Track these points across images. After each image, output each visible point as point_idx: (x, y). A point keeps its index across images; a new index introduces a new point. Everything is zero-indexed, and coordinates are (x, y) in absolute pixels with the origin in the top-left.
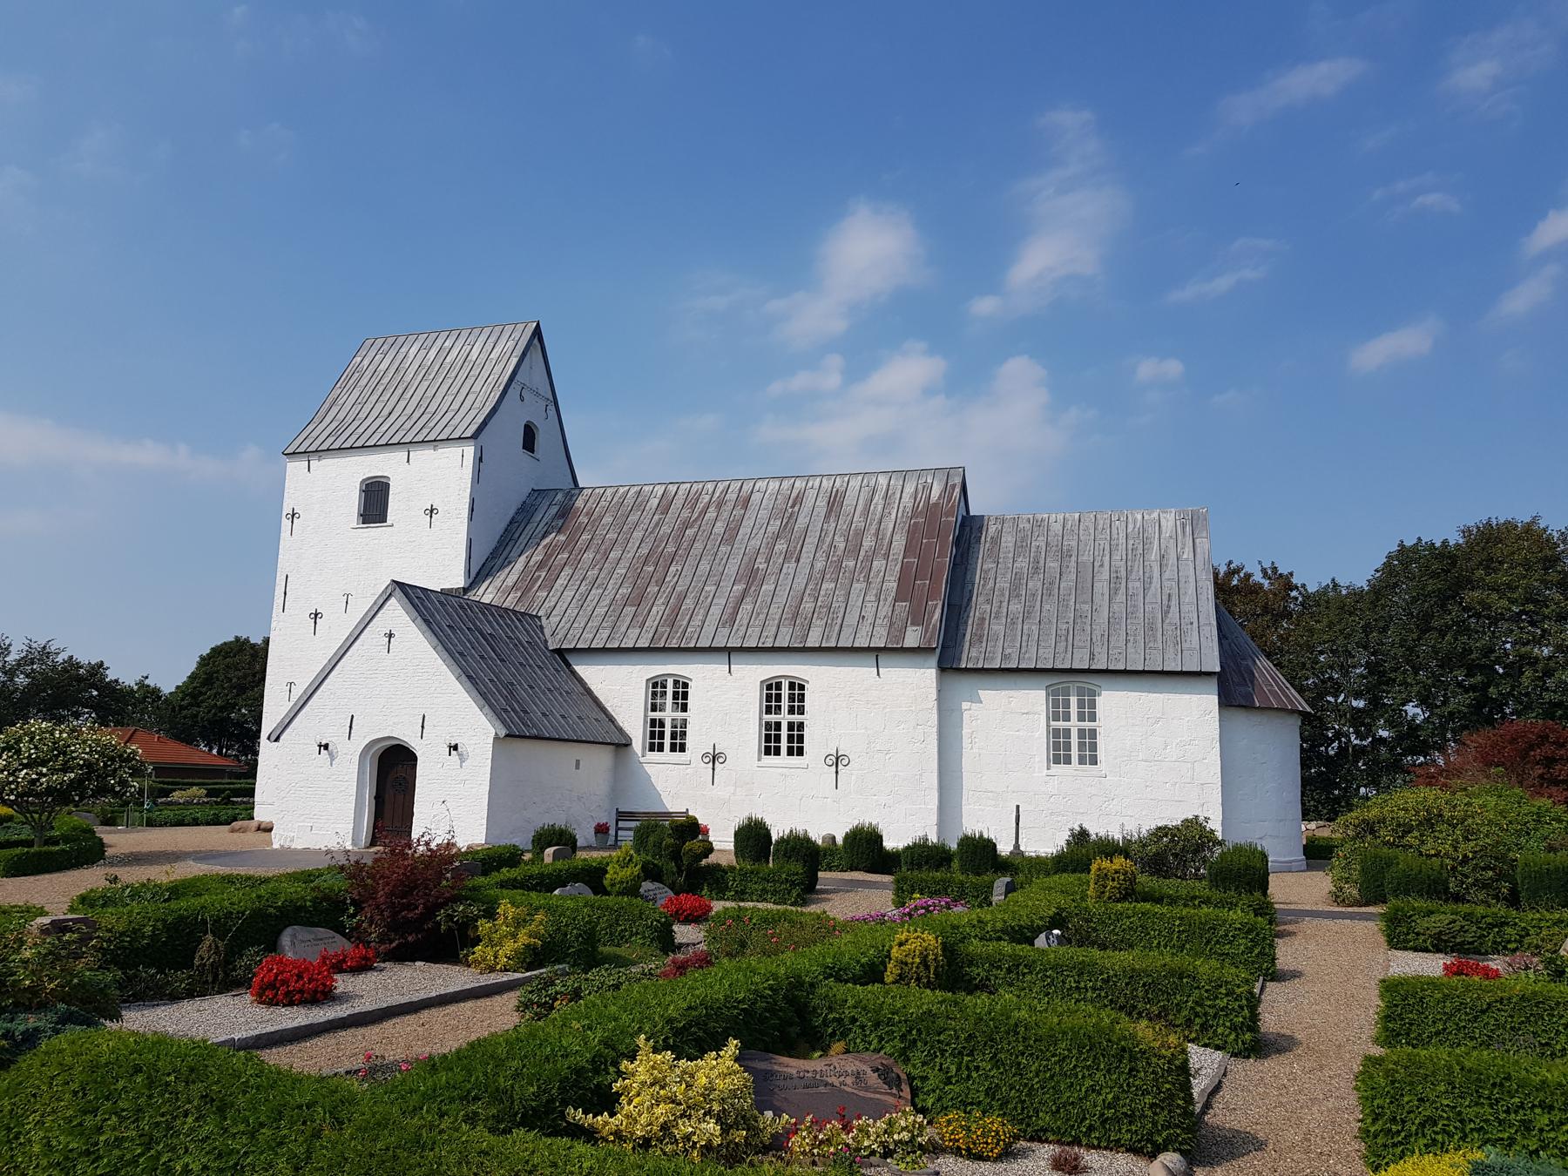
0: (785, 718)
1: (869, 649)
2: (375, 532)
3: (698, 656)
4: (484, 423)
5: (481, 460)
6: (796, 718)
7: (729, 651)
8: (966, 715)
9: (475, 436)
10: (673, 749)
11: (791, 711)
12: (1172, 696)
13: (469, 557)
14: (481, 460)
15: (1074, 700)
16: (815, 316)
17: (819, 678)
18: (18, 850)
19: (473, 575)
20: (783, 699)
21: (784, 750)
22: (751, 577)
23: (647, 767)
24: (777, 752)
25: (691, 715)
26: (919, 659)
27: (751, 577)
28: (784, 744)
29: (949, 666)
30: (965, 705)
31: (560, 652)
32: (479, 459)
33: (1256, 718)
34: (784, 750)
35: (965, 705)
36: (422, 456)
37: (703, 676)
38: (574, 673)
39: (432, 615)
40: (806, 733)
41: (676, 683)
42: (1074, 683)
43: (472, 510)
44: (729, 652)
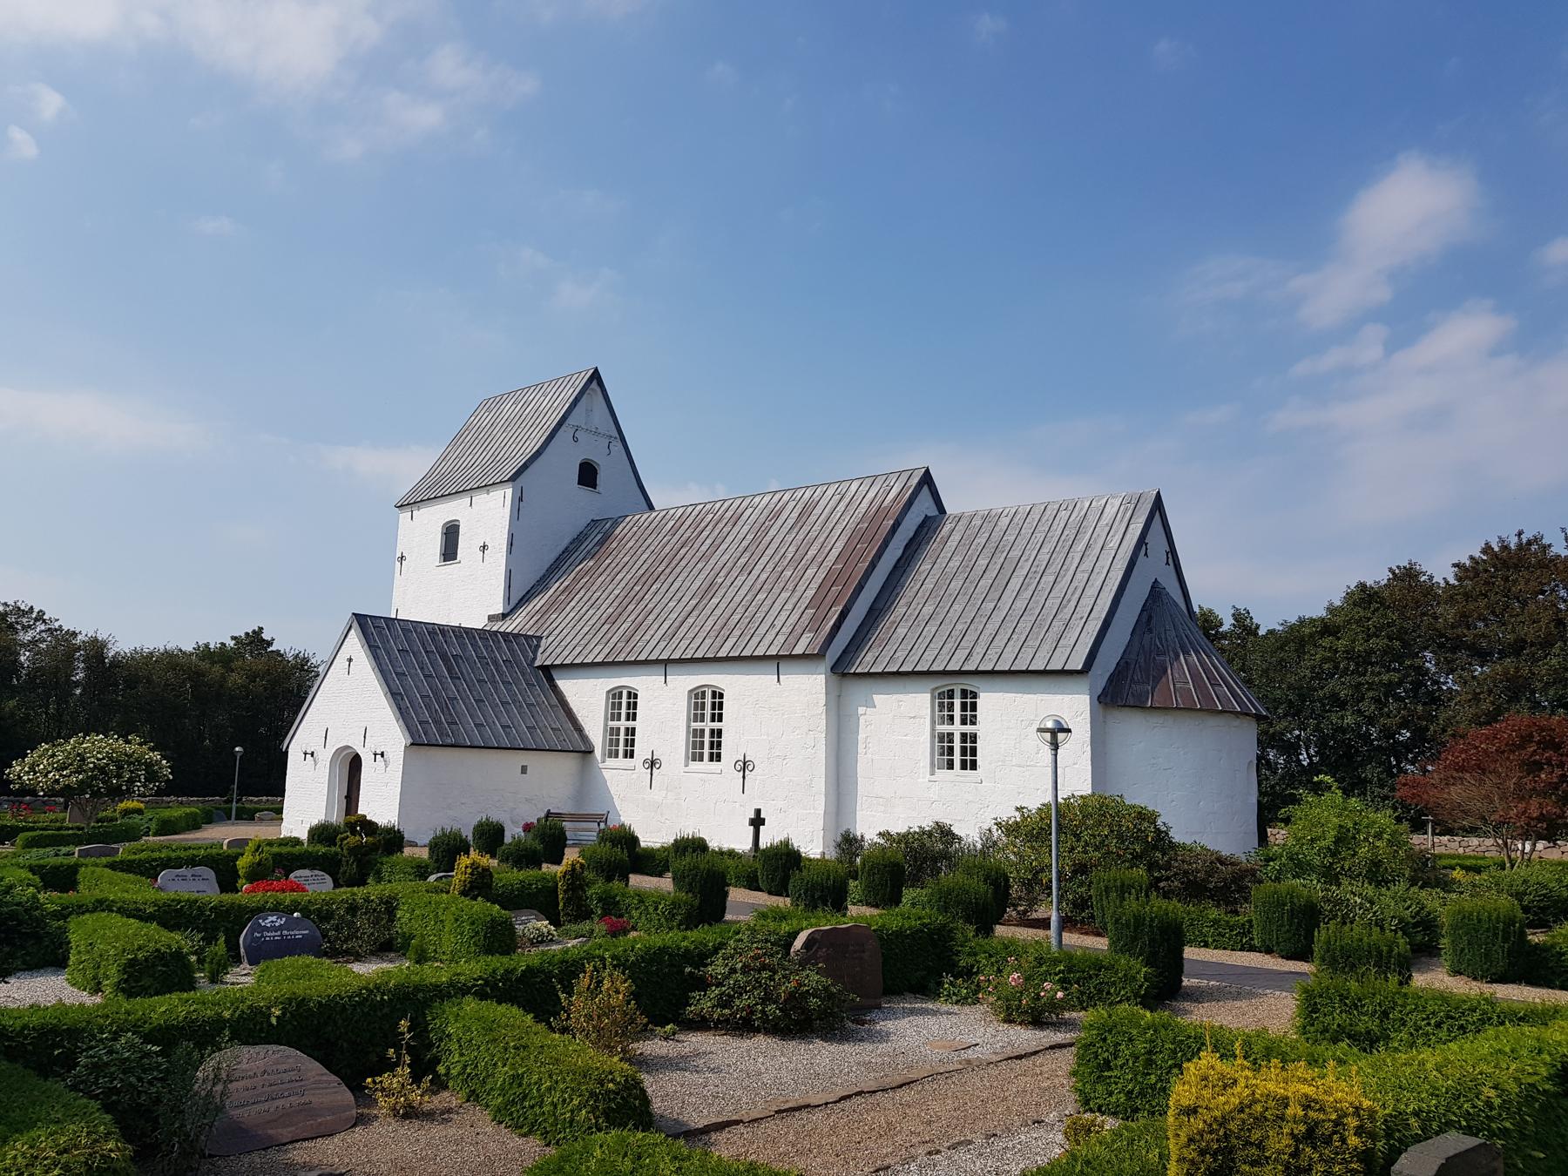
0: (708, 725)
1: (657, 662)
2: (451, 568)
3: (581, 672)
4: (525, 467)
5: (521, 499)
6: (968, 728)
7: (667, 663)
8: (862, 720)
9: (513, 479)
10: (964, 767)
11: (964, 722)
12: (1045, 697)
13: (509, 587)
14: (521, 499)
15: (957, 702)
16: (1335, 292)
17: (732, 683)
18: (38, 833)
19: (514, 601)
20: (709, 705)
21: (706, 756)
22: (710, 589)
23: (607, 774)
24: (617, 756)
25: (637, 724)
26: (810, 665)
27: (710, 589)
28: (957, 758)
29: (843, 670)
30: (861, 710)
31: (547, 670)
32: (519, 499)
33: (1156, 720)
34: (706, 756)
35: (861, 710)
36: (481, 499)
37: (645, 684)
38: (555, 688)
39: (385, 641)
40: (979, 745)
41: (714, 693)
42: (958, 685)
43: (511, 544)
44: (666, 664)
